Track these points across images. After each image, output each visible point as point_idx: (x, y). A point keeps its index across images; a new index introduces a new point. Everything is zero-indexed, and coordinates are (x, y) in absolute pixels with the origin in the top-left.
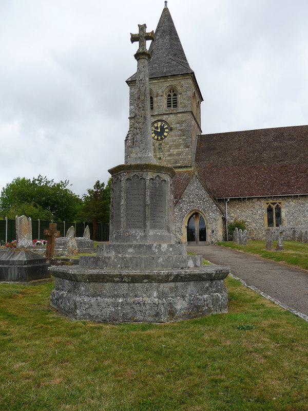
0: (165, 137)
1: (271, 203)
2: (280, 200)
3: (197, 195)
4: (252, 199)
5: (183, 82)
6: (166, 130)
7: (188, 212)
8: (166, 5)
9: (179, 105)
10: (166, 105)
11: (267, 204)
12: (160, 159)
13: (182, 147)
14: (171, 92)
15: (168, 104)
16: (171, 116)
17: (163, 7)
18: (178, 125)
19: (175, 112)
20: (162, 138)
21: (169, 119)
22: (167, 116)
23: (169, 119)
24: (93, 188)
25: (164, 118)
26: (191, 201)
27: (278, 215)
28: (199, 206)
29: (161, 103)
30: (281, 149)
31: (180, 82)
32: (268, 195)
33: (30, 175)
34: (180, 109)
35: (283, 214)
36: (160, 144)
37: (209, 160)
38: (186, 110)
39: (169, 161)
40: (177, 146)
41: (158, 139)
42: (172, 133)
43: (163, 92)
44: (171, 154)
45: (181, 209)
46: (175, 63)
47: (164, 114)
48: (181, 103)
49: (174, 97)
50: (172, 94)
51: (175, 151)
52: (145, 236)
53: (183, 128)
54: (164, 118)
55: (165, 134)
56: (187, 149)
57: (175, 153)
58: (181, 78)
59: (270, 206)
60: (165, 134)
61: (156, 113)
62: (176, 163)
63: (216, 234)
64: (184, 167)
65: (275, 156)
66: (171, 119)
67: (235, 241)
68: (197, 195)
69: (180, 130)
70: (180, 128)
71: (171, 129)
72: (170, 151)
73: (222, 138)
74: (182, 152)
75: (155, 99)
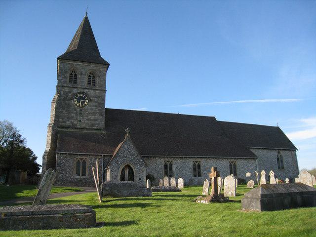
0: (85, 105)
2: (172, 159)
6: (86, 101)
9: (97, 84)
10: (87, 83)
25: (86, 91)
27: (171, 169)
29: (83, 80)
33: (282, 128)
35: (174, 169)
36: (81, 110)
39: (87, 124)
40: (94, 114)
42: (91, 103)
43: (86, 72)
45: (117, 162)
47: (85, 88)
48: (99, 83)
50: (92, 76)
51: (92, 117)
54: (86, 91)
56: (102, 117)
60: (86, 103)
66: (91, 92)
69: (97, 102)
71: (90, 101)
75: (79, 76)
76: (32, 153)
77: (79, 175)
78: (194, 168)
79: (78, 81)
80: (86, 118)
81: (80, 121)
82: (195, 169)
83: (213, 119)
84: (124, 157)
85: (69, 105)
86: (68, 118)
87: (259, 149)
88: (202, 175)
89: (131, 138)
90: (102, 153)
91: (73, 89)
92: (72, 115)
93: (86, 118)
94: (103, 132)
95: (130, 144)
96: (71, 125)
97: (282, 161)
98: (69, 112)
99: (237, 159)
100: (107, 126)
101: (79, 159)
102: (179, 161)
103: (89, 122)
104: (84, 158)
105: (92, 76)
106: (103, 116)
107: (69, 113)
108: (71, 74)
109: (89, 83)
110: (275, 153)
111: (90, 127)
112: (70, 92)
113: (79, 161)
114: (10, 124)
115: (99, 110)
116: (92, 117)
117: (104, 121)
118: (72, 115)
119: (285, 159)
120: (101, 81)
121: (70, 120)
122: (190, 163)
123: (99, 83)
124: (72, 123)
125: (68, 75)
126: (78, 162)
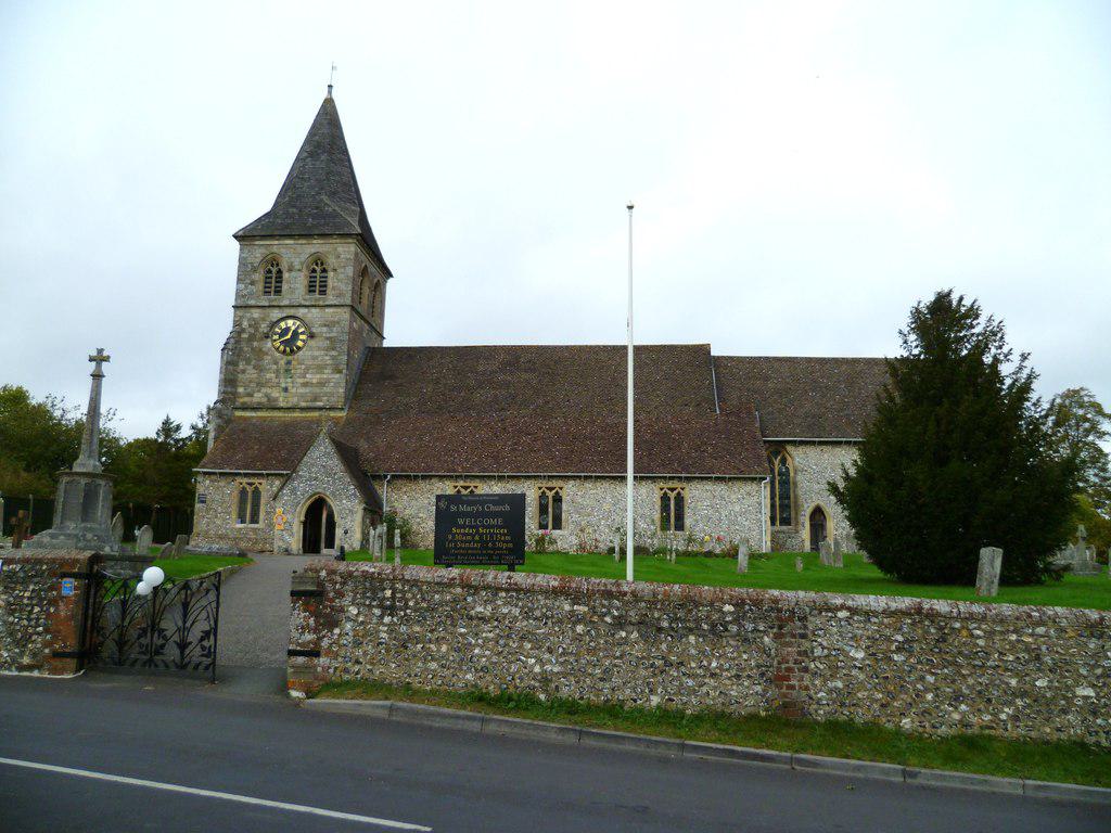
0: (299, 348)
1: (669, 489)
4: (431, 477)
5: (340, 249)
8: (330, 92)
11: (661, 489)
12: (286, 390)
14: (317, 264)
16: (313, 310)
17: (325, 95)
18: (325, 329)
19: (321, 303)
20: (292, 351)
21: (309, 315)
22: (306, 310)
23: (309, 315)
25: (301, 312)
34: (331, 299)
36: (289, 363)
38: (342, 302)
40: (320, 368)
41: (285, 351)
42: (312, 343)
43: (302, 264)
45: (293, 491)
49: (323, 275)
50: (318, 269)
51: (313, 378)
53: (331, 335)
55: (300, 343)
56: (337, 376)
57: (314, 381)
59: (665, 494)
60: (300, 343)
64: (330, 409)
67: (1082, 739)
69: (327, 338)
71: (312, 336)
72: (305, 377)
73: (410, 356)
74: (328, 381)
75: (286, 275)
77: (243, 522)
78: (541, 505)
79: (285, 287)
80: (301, 381)
81: (286, 390)
83: (703, 350)
84: (310, 479)
85: (261, 350)
86: (258, 384)
87: (840, 443)
91: (268, 310)
92: (268, 376)
93: (301, 381)
95: (326, 448)
96: (265, 400)
99: (689, 479)
100: (355, 394)
104: (553, 483)
105: (318, 269)
106: (340, 372)
107: (261, 371)
112: (264, 319)
115: (333, 358)
116: (313, 378)
117: (343, 384)
118: (268, 376)
121: (264, 390)
124: (266, 395)
125: (259, 276)
126: (243, 492)
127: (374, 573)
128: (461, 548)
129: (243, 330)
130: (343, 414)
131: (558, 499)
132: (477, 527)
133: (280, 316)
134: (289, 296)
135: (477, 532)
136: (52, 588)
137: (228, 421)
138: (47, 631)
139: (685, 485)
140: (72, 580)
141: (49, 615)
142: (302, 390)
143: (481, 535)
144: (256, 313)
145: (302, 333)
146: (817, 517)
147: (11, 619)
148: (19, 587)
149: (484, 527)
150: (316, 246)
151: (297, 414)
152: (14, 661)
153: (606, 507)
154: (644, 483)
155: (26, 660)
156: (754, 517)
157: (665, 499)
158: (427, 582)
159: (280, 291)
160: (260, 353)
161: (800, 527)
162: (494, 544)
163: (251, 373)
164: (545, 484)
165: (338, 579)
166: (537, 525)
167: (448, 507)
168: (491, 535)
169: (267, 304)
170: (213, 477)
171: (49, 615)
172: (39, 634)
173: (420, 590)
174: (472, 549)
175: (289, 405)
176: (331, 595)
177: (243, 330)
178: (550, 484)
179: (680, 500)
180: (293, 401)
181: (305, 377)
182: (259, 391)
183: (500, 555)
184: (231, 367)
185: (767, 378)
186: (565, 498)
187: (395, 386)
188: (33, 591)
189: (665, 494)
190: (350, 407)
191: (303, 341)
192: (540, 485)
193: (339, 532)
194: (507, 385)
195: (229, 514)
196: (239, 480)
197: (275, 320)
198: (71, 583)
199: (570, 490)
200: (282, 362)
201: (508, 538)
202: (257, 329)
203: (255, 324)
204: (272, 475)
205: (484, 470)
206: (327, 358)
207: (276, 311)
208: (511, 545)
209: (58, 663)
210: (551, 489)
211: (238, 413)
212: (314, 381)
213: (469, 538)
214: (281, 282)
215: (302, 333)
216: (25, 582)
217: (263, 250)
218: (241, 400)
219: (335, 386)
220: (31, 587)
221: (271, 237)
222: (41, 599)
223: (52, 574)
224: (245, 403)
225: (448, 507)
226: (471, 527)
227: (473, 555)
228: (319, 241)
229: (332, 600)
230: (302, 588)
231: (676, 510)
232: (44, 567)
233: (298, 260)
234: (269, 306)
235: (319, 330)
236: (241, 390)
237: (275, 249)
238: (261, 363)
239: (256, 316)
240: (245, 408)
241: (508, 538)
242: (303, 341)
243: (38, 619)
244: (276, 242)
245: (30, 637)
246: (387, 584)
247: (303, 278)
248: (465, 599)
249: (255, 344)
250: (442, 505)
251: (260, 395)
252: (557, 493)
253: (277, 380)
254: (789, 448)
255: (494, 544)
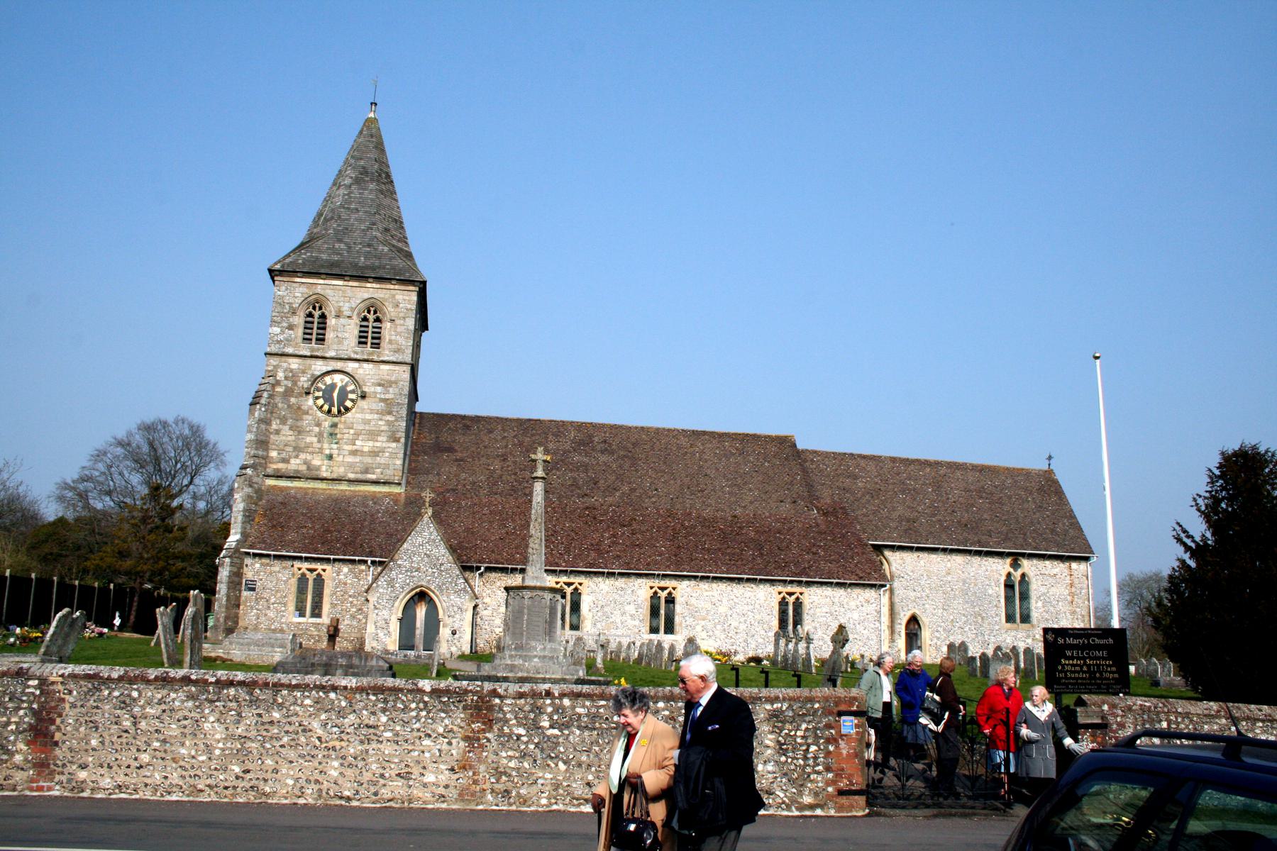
0: (347, 409)
1: (660, 588)
3: (428, 556)
7: (407, 589)
9: (384, 344)
10: (356, 341)
12: (330, 457)
13: (383, 438)
14: (369, 312)
15: (360, 337)
16: (365, 365)
18: (379, 389)
19: (375, 358)
23: (361, 371)
24: (54, 490)
25: (350, 367)
26: (414, 567)
28: (427, 579)
30: (586, 471)
31: (394, 296)
32: (561, 566)
34: (386, 353)
36: (334, 425)
37: (438, 474)
38: (400, 358)
39: (351, 465)
40: (373, 435)
42: (361, 403)
43: (353, 310)
44: (356, 451)
45: (391, 583)
46: (386, 249)
48: (390, 342)
50: (371, 317)
51: (364, 445)
52: (545, 648)
53: (387, 396)
54: (350, 367)
56: (394, 445)
57: (366, 449)
58: (397, 287)
60: (348, 404)
61: (332, 354)
62: (366, 471)
63: (460, 637)
64: (384, 483)
65: (575, 485)
68: (428, 556)
70: (383, 396)
72: (354, 445)
73: (468, 427)
74: (383, 451)
75: (331, 322)
76: (966, 464)
77: (302, 615)
79: (330, 335)
81: (330, 457)
82: (654, 612)
83: (785, 443)
85: (299, 408)
88: (677, 628)
89: (436, 517)
90: (371, 554)
91: (309, 361)
94: (397, 490)
96: (304, 468)
97: (1025, 597)
98: (299, 431)
99: (809, 584)
100: (413, 469)
101: (304, 570)
102: (604, 585)
103: (357, 459)
104: (319, 566)
105: (371, 317)
106: (397, 440)
107: (300, 433)
108: (310, 315)
109: (362, 341)
110: (1000, 567)
111: (360, 476)
112: (304, 372)
113: (303, 575)
114: (196, 431)
116: (364, 445)
118: (308, 439)
119: (1036, 588)
120: (398, 334)
121: (303, 456)
122: (641, 590)
123: (390, 342)
124: (306, 462)
125: (299, 320)
126: (303, 580)
127: (1150, 707)
128: (1071, 678)
129: (278, 383)
130: (397, 490)
131: (670, 600)
132: (1084, 658)
133: (325, 369)
134: (335, 347)
135: (1085, 663)
136: (828, 726)
137: (259, 492)
138: (828, 769)
139: (804, 589)
140: (852, 718)
141: (828, 753)
142: (350, 459)
143: (1089, 666)
144: (294, 364)
145: (353, 392)
146: (912, 626)
147: (783, 759)
148: (788, 726)
149: (1091, 659)
150: (371, 290)
151: (344, 487)
152: (793, 801)
153: (723, 609)
154: (762, 586)
155: (807, 799)
156: (873, 626)
157: (783, 603)
158: (1197, 714)
159: (323, 340)
160: (299, 412)
161: (896, 636)
162: (1101, 674)
163: (287, 435)
164: (657, 583)
165: (1120, 712)
166: (648, 628)
167: (1056, 640)
168: (1098, 666)
169: (309, 354)
170: (265, 561)
171: (828, 753)
172: (818, 773)
173: (1191, 721)
174: (1082, 678)
175: (335, 476)
176: (1115, 726)
177: (278, 383)
178: (571, 580)
179: (798, 605)
180: (340, 471)
181: (354, 445)
182: (297, 457)
183: (1108, 685)
184: (263, 426)
185: (855, 477)
186: (679, 600)
187: (457, 460)
188: (807, 729)
189: (784, 598)
190: (408, 483)
191: (352, 400)
192: (653, 585)
193: (444, 632)
194: (586, 467)
195: (285, 605)
196: (297, 564)
197: (319, 373)
198: (852, 721)
199: (685, 591)
200: (326, 424)
201: (1114, 669)
202: (295, 383)
203: (293, 376)
204: (340, 560)
205: (591, 566)
206: (380, 423)
207: (320, 362)
208: (1116, 676)
209: (844, 800)
210: (663, 589)
211: (271, 482)
212: (366, 449)
213: (1078, 668)
214: (324, 329)
215: (353, 392)
216: (797, 719)
217: (303, 289)
218: (275, 466)
219: (391, 459)
220: (804, 726)
221: (316, 274)
222: (816, 737)
223: (826, 712)
224: (278, 470)
225: (1056, 640)
226: (1078, 658)
227: (1082, 684)
228: (374, 285)
229: (1115, 732)
230: (1089, 722)
231: (794, 616)
232: (817, 706)
233: (347, 304)
234: (312, 357)
235: (372, 389)
236: (274, 454)
237: (319, 290)
238: (299, 424)
239: (294, 366)
240: (278, 476)
241: (1114, 669)
242: (352, 400)
243: (815, 758)
244: (321, 281)
245: (809, 776)
246: (1162, 716)
247: (352, 326)
248: (1230, 729)
249: (293, 400)
250: (1050, 637)
251: (298, 461)
252: (670, 593)
253: (319, 446)
254: (887, 553)
255: (1101, 674)
